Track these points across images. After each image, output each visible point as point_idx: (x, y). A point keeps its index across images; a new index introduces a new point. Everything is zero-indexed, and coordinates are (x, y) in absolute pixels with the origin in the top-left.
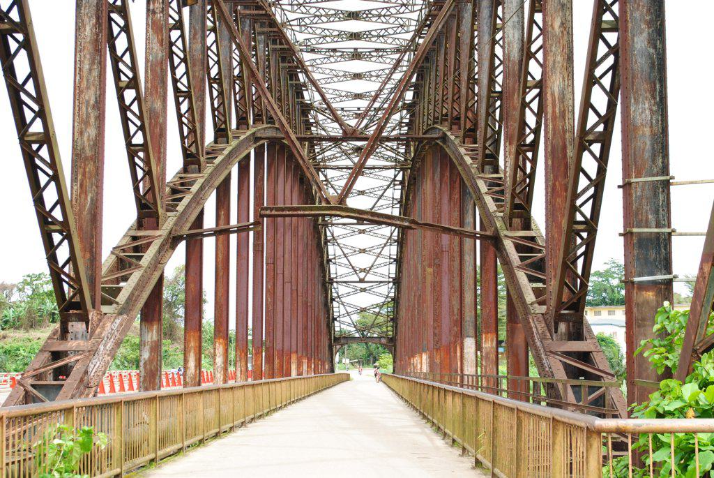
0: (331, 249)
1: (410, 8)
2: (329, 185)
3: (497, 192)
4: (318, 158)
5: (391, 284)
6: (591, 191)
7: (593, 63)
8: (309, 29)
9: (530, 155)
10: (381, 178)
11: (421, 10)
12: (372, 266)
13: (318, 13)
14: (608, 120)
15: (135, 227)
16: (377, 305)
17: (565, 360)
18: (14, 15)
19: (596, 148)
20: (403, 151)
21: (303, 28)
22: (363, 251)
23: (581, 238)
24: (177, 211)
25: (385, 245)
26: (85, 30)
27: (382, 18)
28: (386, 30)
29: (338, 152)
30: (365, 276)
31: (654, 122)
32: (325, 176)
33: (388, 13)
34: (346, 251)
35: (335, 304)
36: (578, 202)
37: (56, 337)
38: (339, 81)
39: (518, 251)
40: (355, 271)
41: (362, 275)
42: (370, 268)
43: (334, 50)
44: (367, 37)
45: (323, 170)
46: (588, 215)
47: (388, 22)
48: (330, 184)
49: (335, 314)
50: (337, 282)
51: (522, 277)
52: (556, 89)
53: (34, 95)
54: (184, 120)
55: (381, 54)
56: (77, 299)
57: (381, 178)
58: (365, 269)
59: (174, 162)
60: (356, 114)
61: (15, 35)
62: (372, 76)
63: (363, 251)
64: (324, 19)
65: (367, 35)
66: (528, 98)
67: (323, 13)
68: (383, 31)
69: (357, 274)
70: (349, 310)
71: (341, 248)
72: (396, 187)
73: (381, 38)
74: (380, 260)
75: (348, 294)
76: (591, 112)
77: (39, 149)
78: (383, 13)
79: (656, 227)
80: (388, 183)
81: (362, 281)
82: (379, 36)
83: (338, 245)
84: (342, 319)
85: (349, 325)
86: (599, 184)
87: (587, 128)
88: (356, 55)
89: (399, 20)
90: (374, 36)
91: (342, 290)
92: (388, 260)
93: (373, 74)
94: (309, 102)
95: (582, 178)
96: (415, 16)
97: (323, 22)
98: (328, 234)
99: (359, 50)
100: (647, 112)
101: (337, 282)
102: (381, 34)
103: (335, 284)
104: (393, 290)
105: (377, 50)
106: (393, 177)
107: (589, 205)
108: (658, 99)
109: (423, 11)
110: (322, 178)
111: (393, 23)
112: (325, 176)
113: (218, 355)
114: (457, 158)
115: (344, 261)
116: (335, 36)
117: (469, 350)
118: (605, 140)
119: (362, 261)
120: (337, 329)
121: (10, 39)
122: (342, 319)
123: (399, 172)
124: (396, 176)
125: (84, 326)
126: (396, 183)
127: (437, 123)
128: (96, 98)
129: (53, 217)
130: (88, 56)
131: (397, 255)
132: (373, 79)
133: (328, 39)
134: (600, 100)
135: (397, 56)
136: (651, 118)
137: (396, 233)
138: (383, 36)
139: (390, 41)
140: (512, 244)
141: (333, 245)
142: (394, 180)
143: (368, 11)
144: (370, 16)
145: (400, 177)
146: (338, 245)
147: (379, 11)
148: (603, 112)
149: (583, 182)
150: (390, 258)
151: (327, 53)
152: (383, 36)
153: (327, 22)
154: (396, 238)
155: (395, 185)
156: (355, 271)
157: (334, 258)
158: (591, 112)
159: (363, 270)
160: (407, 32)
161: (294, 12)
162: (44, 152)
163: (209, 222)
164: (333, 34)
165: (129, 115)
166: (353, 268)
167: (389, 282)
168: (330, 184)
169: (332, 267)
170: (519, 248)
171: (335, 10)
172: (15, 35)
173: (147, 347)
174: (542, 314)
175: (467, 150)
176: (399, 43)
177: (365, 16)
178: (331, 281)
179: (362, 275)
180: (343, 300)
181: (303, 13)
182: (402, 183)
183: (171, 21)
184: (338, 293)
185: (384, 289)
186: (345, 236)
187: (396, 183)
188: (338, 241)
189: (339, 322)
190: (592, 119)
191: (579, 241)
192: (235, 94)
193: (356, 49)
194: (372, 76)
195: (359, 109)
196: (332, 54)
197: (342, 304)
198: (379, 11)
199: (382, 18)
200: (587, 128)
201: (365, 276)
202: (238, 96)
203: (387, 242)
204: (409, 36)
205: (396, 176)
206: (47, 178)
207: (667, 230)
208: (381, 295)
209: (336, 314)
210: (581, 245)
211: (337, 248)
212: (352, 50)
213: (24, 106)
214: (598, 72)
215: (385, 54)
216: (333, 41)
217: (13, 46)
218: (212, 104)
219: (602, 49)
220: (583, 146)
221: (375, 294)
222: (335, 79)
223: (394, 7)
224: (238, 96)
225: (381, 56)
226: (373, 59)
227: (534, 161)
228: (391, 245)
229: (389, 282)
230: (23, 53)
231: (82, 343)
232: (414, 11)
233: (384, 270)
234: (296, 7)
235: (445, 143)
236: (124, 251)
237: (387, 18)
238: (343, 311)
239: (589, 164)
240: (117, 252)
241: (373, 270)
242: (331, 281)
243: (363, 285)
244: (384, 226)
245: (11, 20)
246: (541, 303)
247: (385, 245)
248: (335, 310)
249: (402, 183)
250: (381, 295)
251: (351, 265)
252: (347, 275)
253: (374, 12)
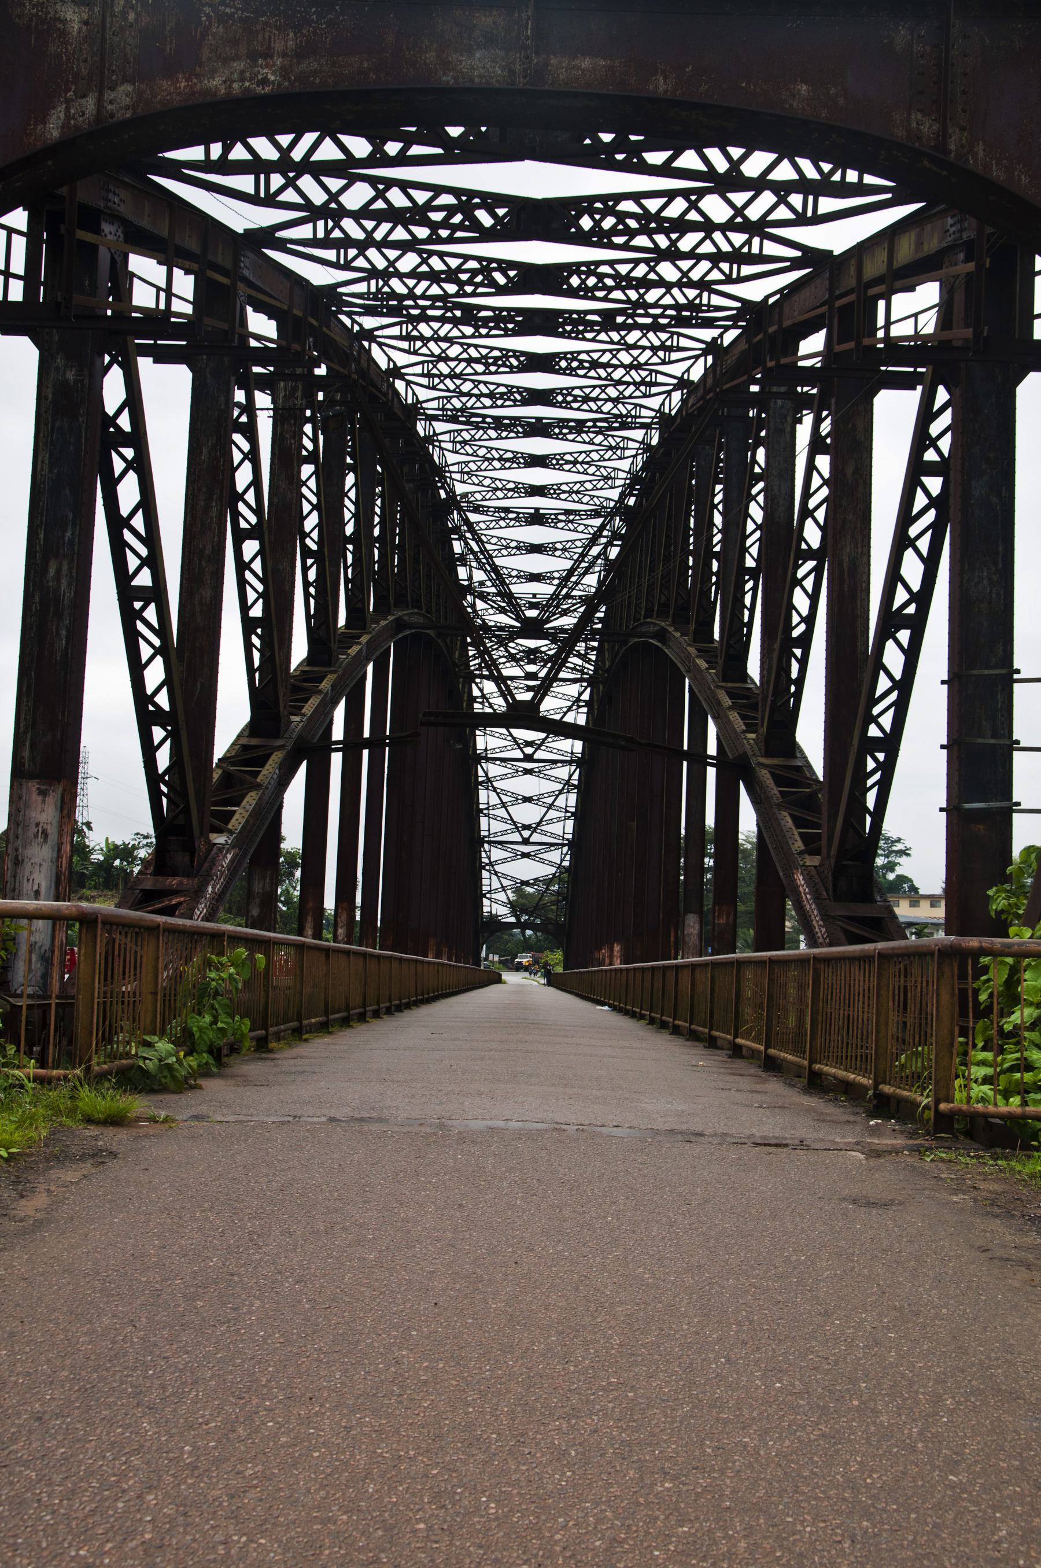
0: (483, 796)
1: (619, 452)
2: (486, 704)
3: (745, 706)
4: (472, 663)
5: (566, 849)
6: (893, 696)
7: (906, 517)
8: (474, 478)
9: (798, 652)
10: (560, 696)
11: (635, 456)
12: (541, 821)
13: (489, 456)
14: (923, 598)
15: (246, 733)
16: (550, 794)
17: (848, 927)
18: (124, 422)
19: (904, 636)
20: (593, 658)
21: (466, 477)
22: (527, 800)
23: (875, 759)
24: (304, 715)
25: (561, 792)
26: (201, 452)
27: (578, 466)
28: (582, 483)
29: (503, 656)
30: (531, 835)
31: (994, 596)
32: (481, 690)
33: (588, 459)
34: (505, 799)
35: (485, 874)
36: (876, 711)
37: (149, 871)
38: (510, 555)
39: (778, 784)
40: (517, 828)
41: (526, 833)
42: (539, 824)
43: (507, 510)
44: (557, 464)
45: (478, 680)
46: (888, 728)
47: (585, 473)
48: (488, 702)
49: (484, 888)
50: (489, 843)
51: (734, 716)
52: (846, 559)
53: (254, 505)
54: (312, 590)
55: (571, 517)
56: (181, 820)
57: (560, 696)
58: (533, 742)
59: (299, 650)
60: (530, 603)
61: (122, 450)
62: (556, 549)
63: (527, 800)
64: (497, 464)
65: (558, 460)
66: (800, 574)
67: (497, 456)
68: (578, 485)
69: (519, 832)
70: (506, 883)
71: (498, 794)
72: (580, 710)
73: (574, 495)
74: (552, 814)
75: (504, 861)
76: (900, 587)
77: (144, 608)
78: (580, 459)
79: (992, 738)
80: (570, 703)
81: (526, 841)
82: (570, 492)
83: (495, 789)
84: (494, 896)
85: (504, 904)
86: (904, 686)
87: (894, 608)
88: (537, 518)
89: (602, 470)
90: (564, 492)
91: (497, 854)
92: (563, 814)
93: (559, 546)
94: (466, 583)
95: (883, 678)
96: (625, 465)
97: (495, 469)
98: (481, 773)
99: (541, 511)
100: (985, 582)
101: (489, 843)
102: (575, 489)
103: (486, 846)
104: (568, 857)
105: (568, 512)
106: (576, 695)
107: (889, 716)
108: (1000, 566)
109: (639, 457)
110: (476, 692)
111: (593, 475)
112: (481, 690)
113: (340, 925)
114: (683, 662)
115: (502, 812)
116: (509, 490)
117: (691, 930)
118: (918, 625)
119: (526, 814)
120: (486, 909)
121: (114, 455)
122: (494, 896)
123: (586, 688)
124: (580, 694)
125: (187, 858)
126: (581, 704)
127: (651, 617)
128: (213, 547)
129: (155, 705)
130: (204, 489)
131: (576, 807)
132: (558, 553)
133: (500, 494)
134: (912, 570)
135: (598, 522)
136: (991, 590)
137: (576, 776)
138: (577, 492)
139: (586, 499)
140: (768, 776)
141: (487, 789)
142: (578, 700)
143: (559, 454)
144: (561, 462)
145: (586, 696)
146: (495, 789)
147: (576, 455)
148: (916, 587)
149: (883, 683)
150: (567, 811)
151: (496, 514)
152: (577, 492)
153: (500, 469)
154: (576, 783)
155: (579, 707)
156: (517, 828)
157: (487, 809)
158: (900, 587)
159: (526, 827)
160: (611, 488)
161: (457, 452)
162: (151, 614)
163: (338, 733)
164: (508, 487)
165: (248, 575)
166: (514, 823)
167: (563, 845)
168: (488, 702)
169: (484, 822)
170: (779, 781)
171: (513, 452)
172: (122, 450)
173: (257, 901)
174: (815, 867)
175: (699, 650)
176: (598, 503)
177: (554, 462)
178: (481, 841)
179: (529, 750)
180: (497, 868)
181: (467, 454)
182: (588, 704)
183: (304, 453)
184: (489, 858)
185: (563, 772)
186: (503, 777)
187: (581, 704)
188: (495, 784)
189: (490, 899)
190: (901, 596)
191: (871, 765)
192: (346, 568)
193: (537, 509)
194: (556, 549)
195: (534, 596)
196: (503, 515)
197: (496, 873)
198: (576, 455)
199: (578, 466)
200: (894, 608)
201: (531, 835)
202: (350, 571)
203: (563, 788)
204: (615, 494)
205: (580, 694)
206: (152, 651)
207: (1006, 742)
208: (551, 863)
209: (485, 888)
210: (873, 772)
211: (493, 795)
212: (532, 511)
213: (128, 551)
214: (913, 531)
215: (578, 517)
216: (506, 497)
217: (119, 466)
218: (346, 574)
219: (920, 500)
220: (886, 631)
221: (543, 861)
222: (504, 552)
223: (587, 490)
224: (350, 571)
225: (572, 522)
226: (560, 525)
227: (803, 663)
228: (568, 792)
229: (563, 845)
230: (132, 477)
231: (185, 881)
232: (625, 458)
233: (557, 828)
234: (458, 446)
235: (664, 643)
236: (234, 764)
237: (586, 466)
238: (496, 884)
239: (893, 658)
240: (225, 765)
241: (542, 828)
242: (481, 841)
243: (526, 849)
244: (559, 765)
245: (118, 428)
246: (813, 852)
247: (561, 792)
248: (484, 882)
249: (588, 704)
250: (551, 863)
251: (512, 819)
252: (505, 832)
253: (568, 457)
